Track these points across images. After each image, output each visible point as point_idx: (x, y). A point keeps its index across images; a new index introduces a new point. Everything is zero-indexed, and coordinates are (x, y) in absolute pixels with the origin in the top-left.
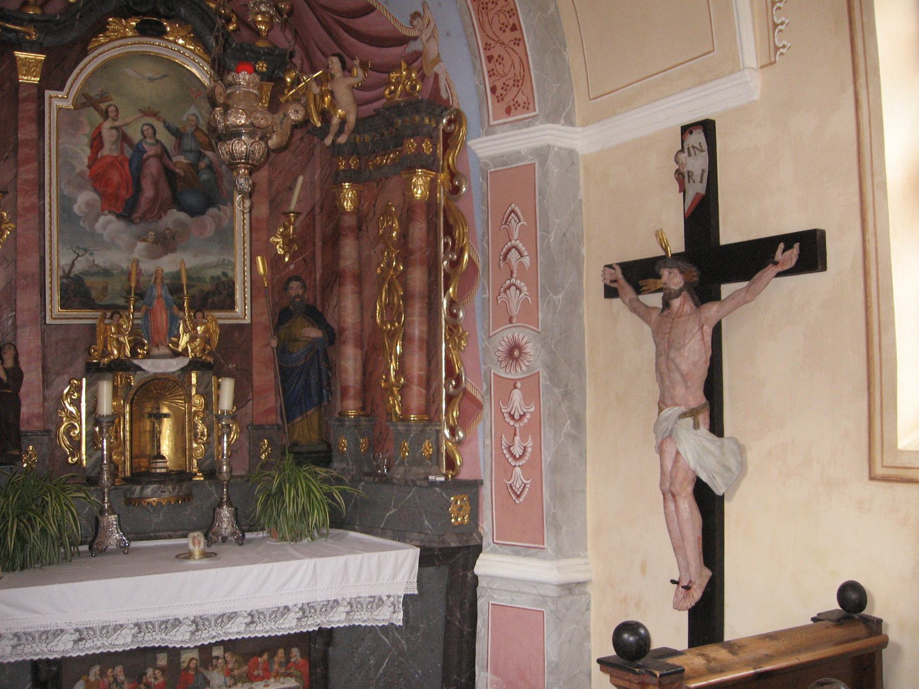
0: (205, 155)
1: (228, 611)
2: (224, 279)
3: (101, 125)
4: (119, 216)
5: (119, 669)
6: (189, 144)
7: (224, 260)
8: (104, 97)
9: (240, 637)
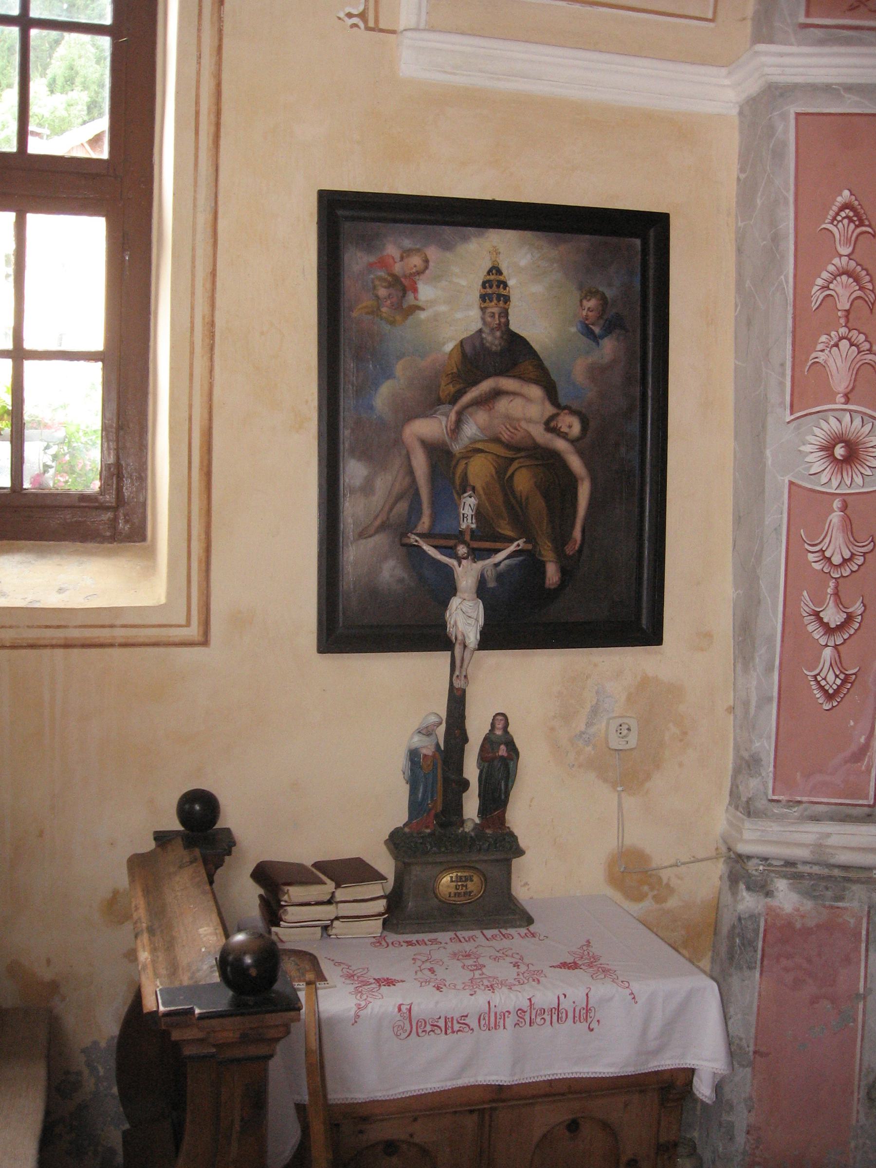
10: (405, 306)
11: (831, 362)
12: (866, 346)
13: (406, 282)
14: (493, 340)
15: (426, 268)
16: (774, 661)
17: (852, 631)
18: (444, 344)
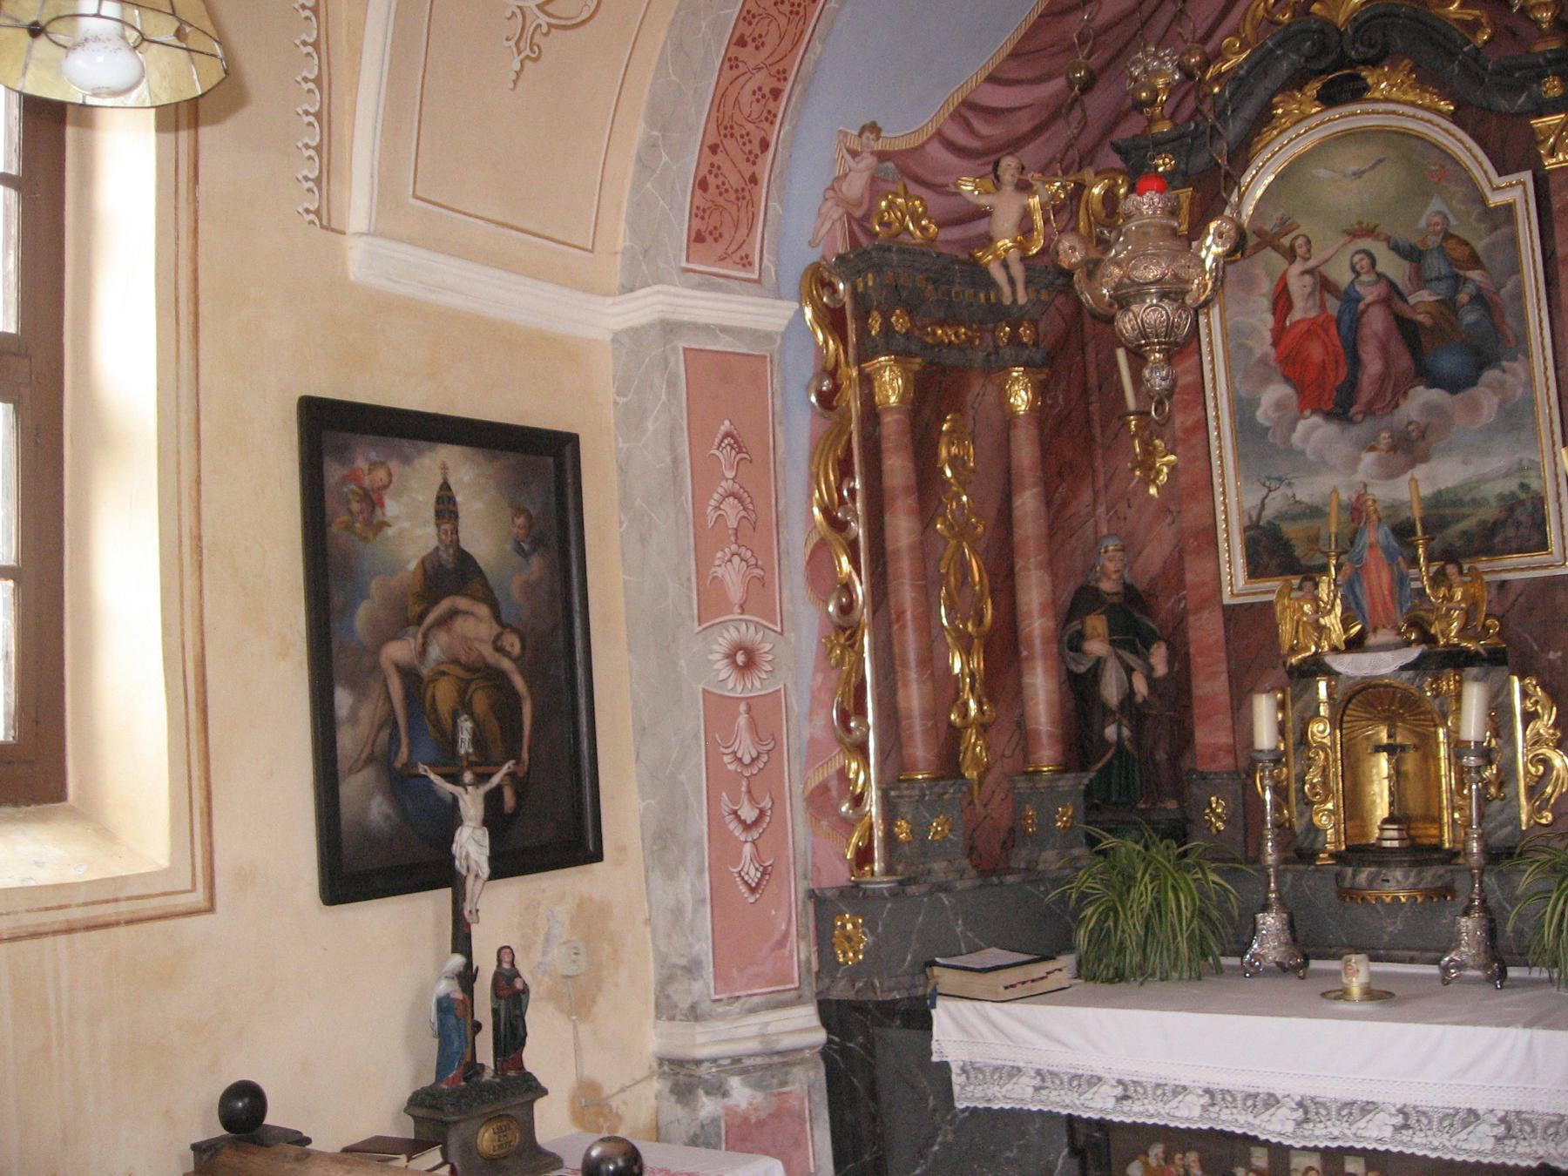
0: (1466, 279)
1: (1360, 1098)
2: (1523, 496)
3: (1285, 273)
4: (1329, 416)
5: (1192, 1157)
6: (1435, 266)
7: (1521, 460)
8: (1286, 226)
9: (1382, 1148)
10: (375, 522)
11: (727, 577)
12: (752, 561)
13: (374, 496)
14: (447, 557)
15: (390, 482)
16: (703, 862)
17: (765, 825)
18: (408, 562)
